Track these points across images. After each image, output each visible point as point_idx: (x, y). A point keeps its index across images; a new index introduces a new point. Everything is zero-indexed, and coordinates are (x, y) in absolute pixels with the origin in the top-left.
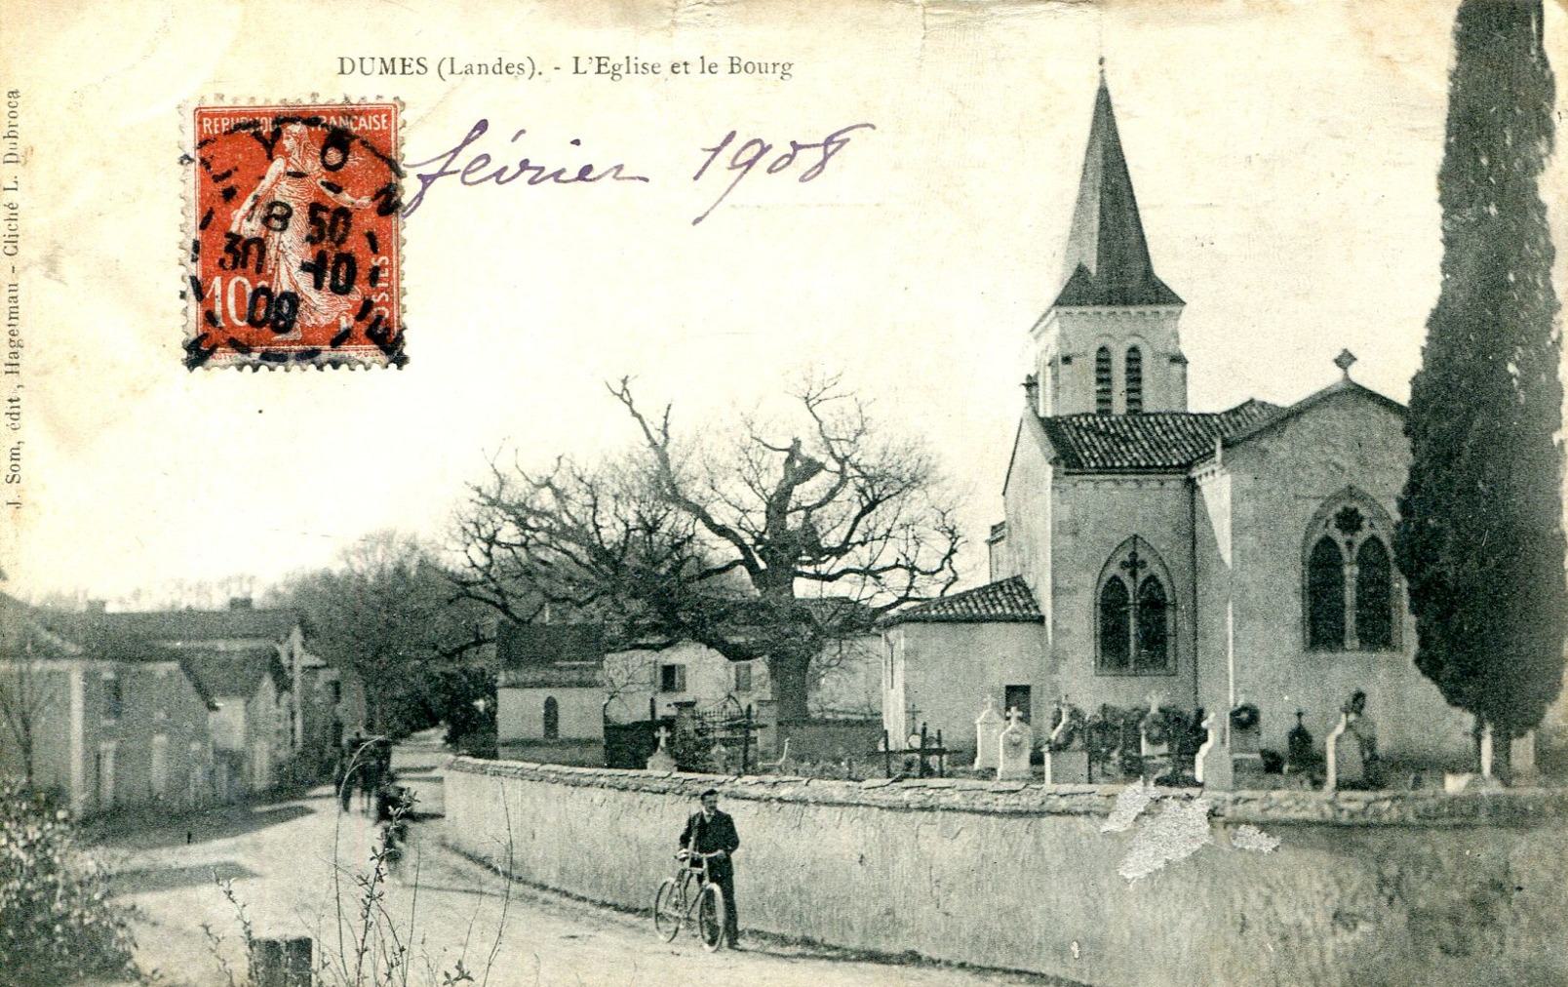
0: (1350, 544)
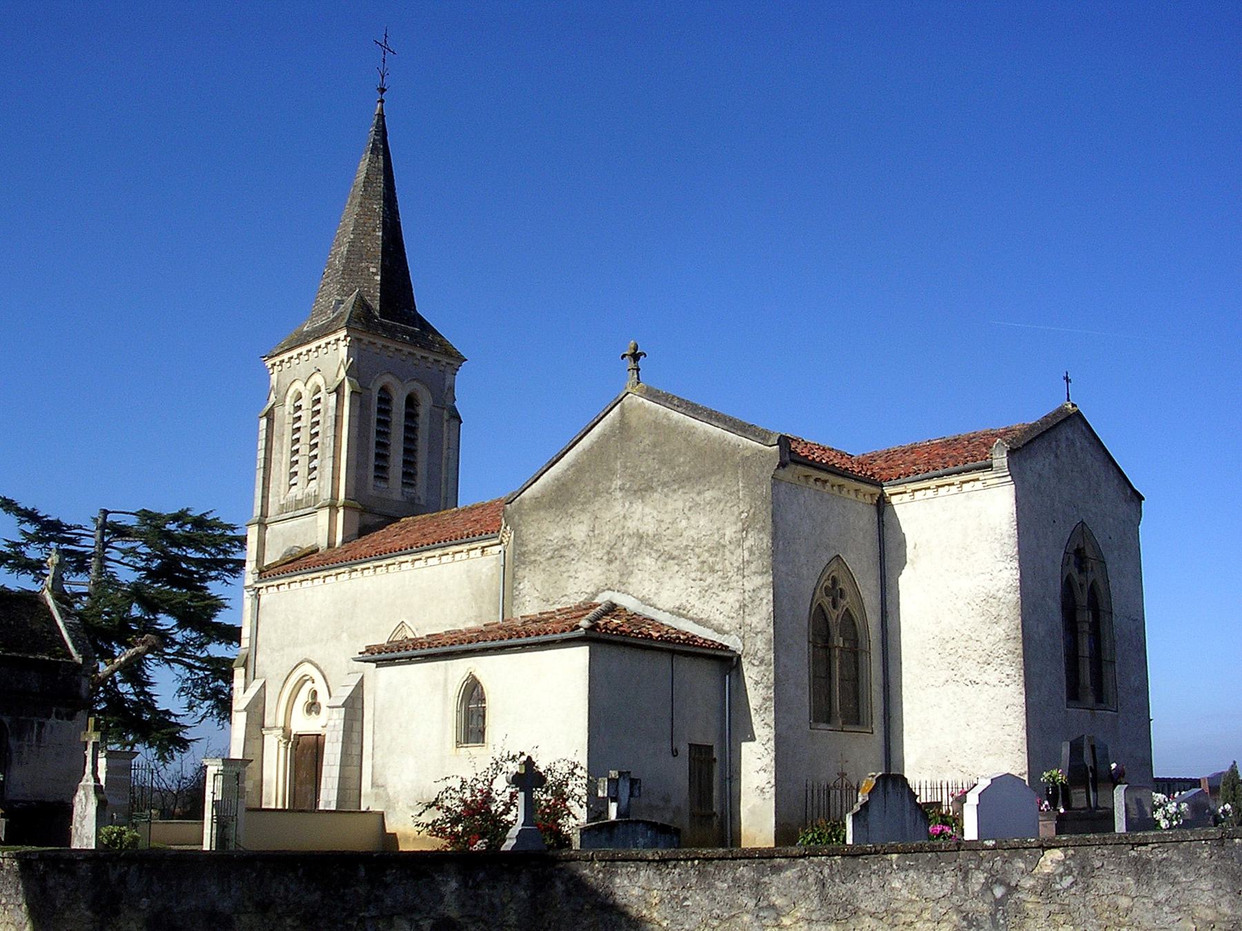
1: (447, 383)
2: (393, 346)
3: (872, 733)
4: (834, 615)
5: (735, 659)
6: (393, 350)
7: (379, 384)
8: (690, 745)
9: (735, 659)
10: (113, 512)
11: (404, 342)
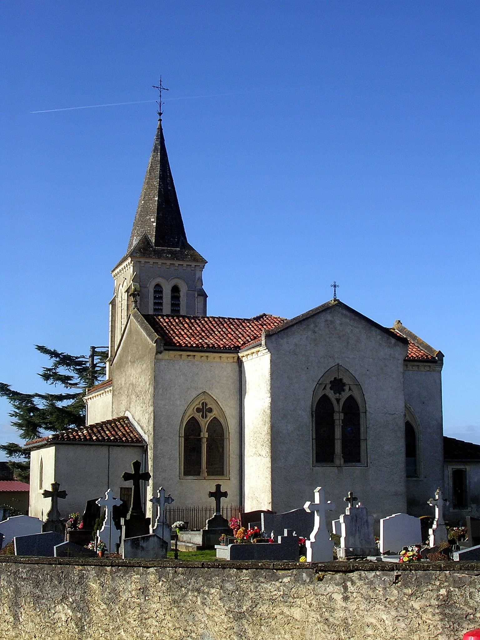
0: (338, 400)
1: (197, 277)
2: (160, 262)
3: (229, 479)
4: (204, 423)
5: (145, 447)
6: (161, 264)
7: (154, 283)
8: (121, 488)
9: (145, 447)
10: (98, 347)
11: (167, 258)
